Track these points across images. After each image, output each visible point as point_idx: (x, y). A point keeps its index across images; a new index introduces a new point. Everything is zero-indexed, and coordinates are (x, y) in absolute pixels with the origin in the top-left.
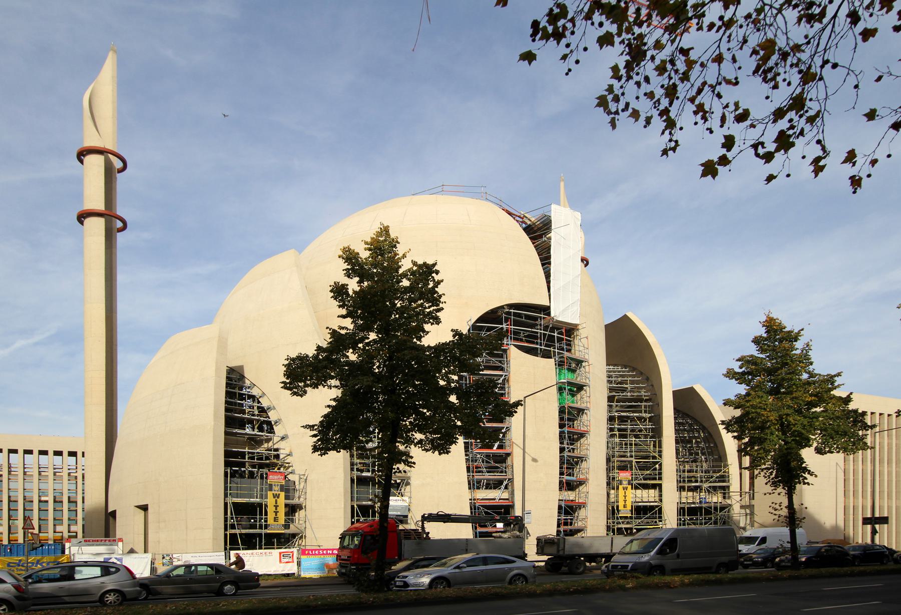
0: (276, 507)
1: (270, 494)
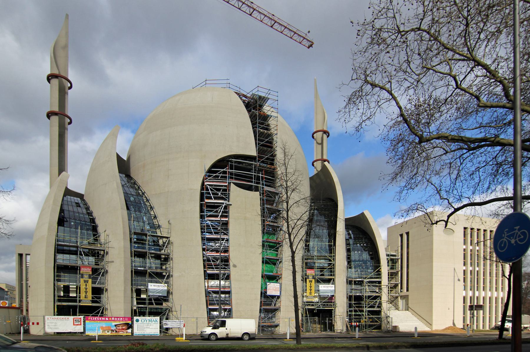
0: (86, 289)
1: (82, 280)
